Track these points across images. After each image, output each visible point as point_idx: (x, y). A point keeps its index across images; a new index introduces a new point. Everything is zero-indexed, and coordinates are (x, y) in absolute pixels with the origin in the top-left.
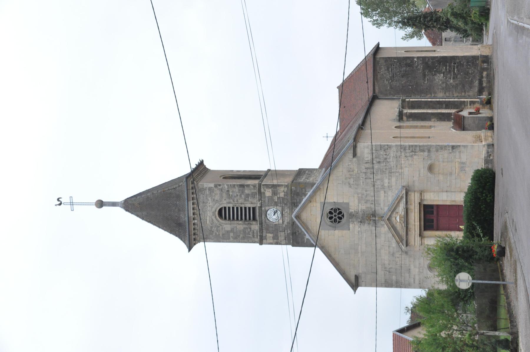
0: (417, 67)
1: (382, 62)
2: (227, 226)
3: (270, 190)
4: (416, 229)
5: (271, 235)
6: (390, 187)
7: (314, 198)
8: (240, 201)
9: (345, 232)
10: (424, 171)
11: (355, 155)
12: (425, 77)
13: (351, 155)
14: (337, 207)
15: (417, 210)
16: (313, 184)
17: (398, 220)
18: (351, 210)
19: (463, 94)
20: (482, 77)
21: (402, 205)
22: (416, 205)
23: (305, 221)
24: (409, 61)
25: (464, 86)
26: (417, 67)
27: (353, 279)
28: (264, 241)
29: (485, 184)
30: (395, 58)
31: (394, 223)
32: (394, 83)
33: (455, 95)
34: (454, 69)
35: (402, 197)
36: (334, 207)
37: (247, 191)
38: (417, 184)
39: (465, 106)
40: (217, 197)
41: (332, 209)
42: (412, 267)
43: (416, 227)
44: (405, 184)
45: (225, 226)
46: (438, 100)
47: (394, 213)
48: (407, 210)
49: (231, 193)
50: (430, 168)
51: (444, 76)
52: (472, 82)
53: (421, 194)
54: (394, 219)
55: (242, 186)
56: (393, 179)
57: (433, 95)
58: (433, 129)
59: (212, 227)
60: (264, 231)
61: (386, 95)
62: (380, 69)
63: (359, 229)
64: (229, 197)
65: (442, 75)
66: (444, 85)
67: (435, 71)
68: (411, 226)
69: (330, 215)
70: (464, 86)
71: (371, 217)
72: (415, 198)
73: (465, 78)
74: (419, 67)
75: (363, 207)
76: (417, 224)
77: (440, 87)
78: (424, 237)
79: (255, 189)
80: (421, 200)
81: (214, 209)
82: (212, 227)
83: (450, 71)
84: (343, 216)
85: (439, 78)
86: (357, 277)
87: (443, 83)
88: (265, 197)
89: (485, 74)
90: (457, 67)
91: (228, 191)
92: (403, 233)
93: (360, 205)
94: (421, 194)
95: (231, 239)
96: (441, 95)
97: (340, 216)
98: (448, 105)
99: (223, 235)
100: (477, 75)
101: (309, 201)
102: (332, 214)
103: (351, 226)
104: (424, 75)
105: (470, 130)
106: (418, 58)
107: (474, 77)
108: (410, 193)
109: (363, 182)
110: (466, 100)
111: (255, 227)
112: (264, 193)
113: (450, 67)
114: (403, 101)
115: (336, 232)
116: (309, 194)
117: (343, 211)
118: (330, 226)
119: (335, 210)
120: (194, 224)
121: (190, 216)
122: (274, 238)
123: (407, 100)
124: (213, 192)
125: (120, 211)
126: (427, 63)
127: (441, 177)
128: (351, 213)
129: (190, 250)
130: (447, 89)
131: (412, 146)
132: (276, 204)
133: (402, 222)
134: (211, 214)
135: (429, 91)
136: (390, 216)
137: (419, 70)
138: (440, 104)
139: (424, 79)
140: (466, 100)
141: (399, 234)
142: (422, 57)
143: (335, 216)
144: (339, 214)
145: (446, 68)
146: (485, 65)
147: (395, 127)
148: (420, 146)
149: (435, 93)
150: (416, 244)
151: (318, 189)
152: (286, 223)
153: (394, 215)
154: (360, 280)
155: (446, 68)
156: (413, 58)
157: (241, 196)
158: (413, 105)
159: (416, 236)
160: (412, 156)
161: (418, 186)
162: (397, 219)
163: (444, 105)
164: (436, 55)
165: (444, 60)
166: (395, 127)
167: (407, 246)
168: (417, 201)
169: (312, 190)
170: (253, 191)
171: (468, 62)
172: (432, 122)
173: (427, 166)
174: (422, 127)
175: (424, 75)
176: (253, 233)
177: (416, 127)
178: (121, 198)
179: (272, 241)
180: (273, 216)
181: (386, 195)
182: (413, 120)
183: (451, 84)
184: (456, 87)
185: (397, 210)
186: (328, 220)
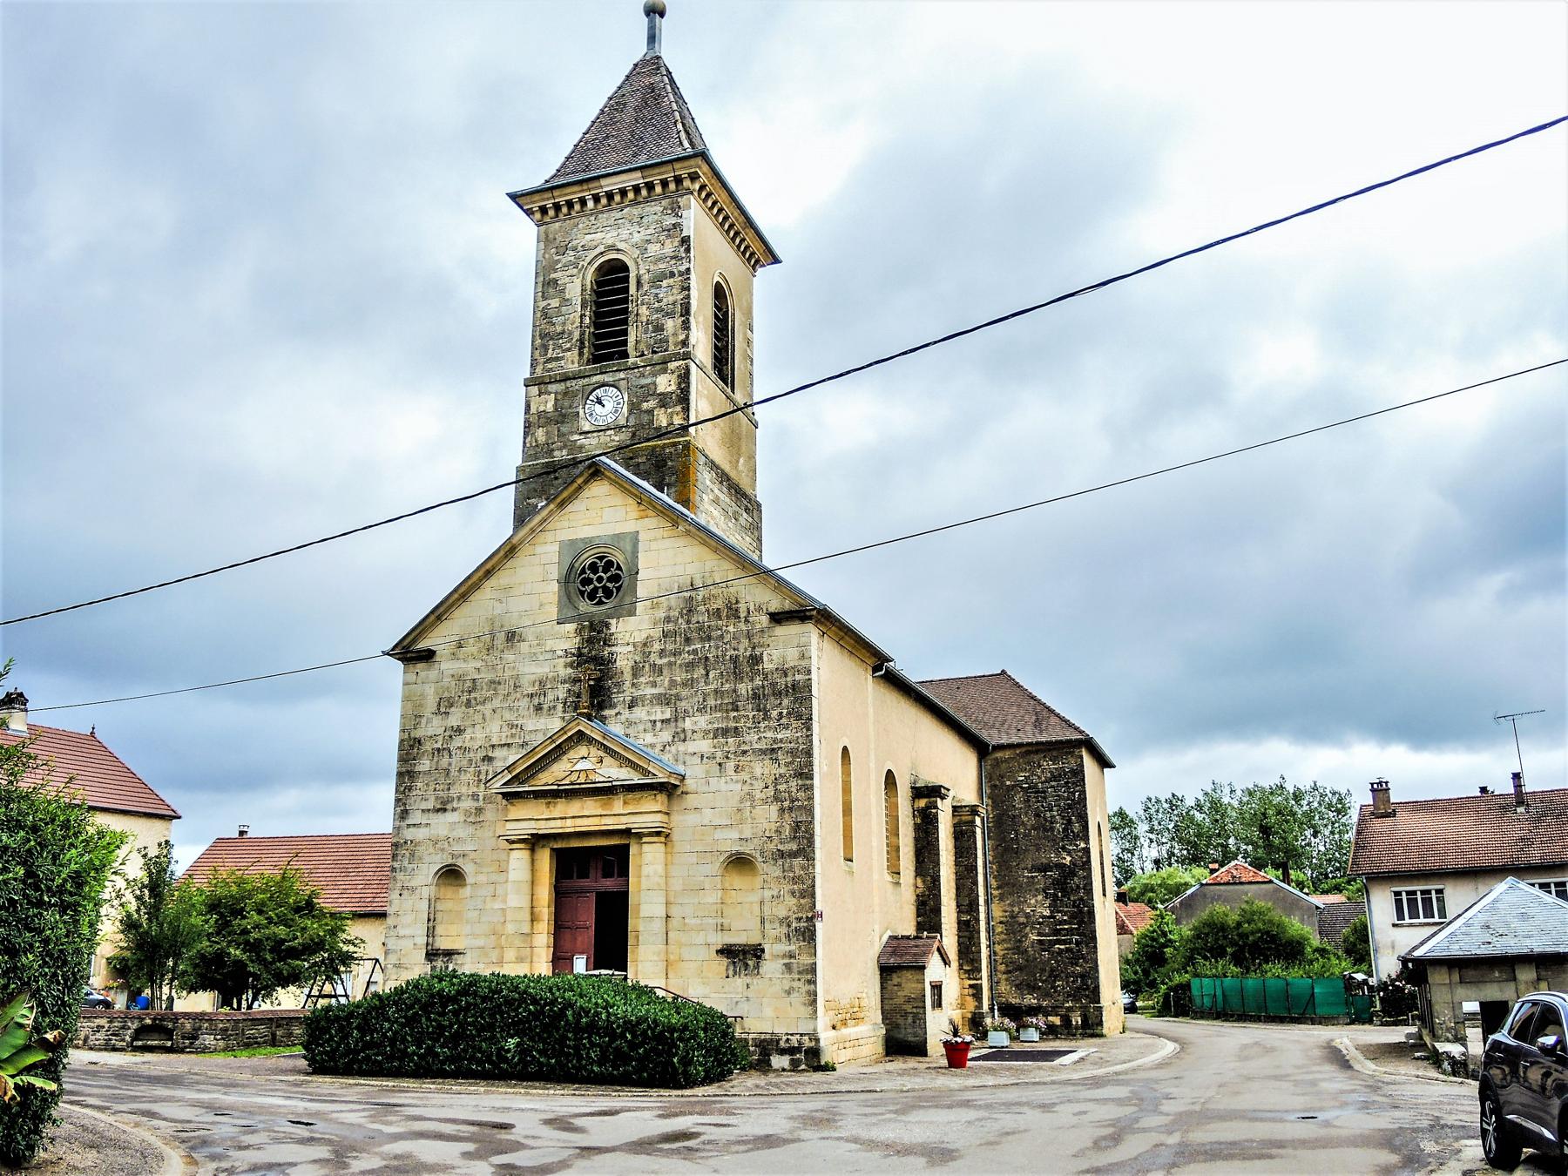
0: (1064, 848)
1: (1073, 763)
2: (577, 286)
3: (674, 387)
4: (552, 824)
5: (550, 407)
6: (681, 736)
7: (650, 513)
8: (644, 310)
9: (553, 612)
10: (729, 842)
11: (778, 618)
12: (1039, 870)
13: (776, 605)
14: (626, 581)
15: (611, 823)
16: (686, 502)
17: (578, 767)
18: (613, 622)
19: (1003, 968)
20: (1046, 1014)
21: (636, 779)
22: (624, 819)
23: (586, 493)
24: (1077, 827)
25: (1020, 968)
26: (1064, 848)
27: (422, 645)
28: (534, 390)
29: (675, 1053)
30: (1083, 792)
31: (572, 754)
32: (1018, 799)
33: (998, 948)
34: (1064, 942)
35: (646, 772)
36: (624, 574)
37: (670, 325)
38: (691, 819)
39: (967, 972)
40: (653, 249)
41: (619, 568)
42: (450, 817)
43: (559, 823)
44: (690, 784)
45: (578, 282)
46: (981, 900)
47: (601, 753)
48: (607, 791)
49: (664, 283)
50: (739, 862)
51: (1043, 917)
52: (1032, 988)
53: (658, 834)
54: (582, 750)
55: (686, 311)
56: (705, 746)
57: (996, 893)
58: (889, 878)
59: (575, 249)
60: (560, 387)
61: (990, 779)
62: (1054, 760)
63: (560, 653)
64: (657, 280)
65: (1047, 913)
66: (1022, 920)
67: (1055, 895)
68: (562, 808)
69: (601, 564)
70: (1020, 968)
71: (595, 686)
72: (644, 813)
73: (1043, 970)
74: (1064, 854)
75: (624, 658)
76: (569, 826)
77: (1016, 909)
78: (533, 850)
79: (676, 345)
80: (639, 836)
81: (621, 246)
82: (575, 249)
83: (1056, 932)
84: (600, 603)
85: (1038, 906)
86: (428, 656)
87: (1027, 916)
88: (655, 375)
89: (1057, 1020)
90: (1068, 950)
91: (672, 275)
92: (545, 780)
93: (630, 648)
94: (658, 834)
95: (542, 304)
96: (997, 912)
97: (600, 594)
98: (967, 931)
99: (555, 281)
100: (1047, 992)
101: (641, 498)
102: (610, 579)
103: (571, 627)
104: (1043, 869)
105: (883, 988)
106: (1087, 851)
107: (1047, 995)
108: (662, 798)
109: (695, 652)
110: (985, 973)
111: (571, 362)
112: (665, 371)
113: (1070, 932)
114: (974, 811)
115: (555, 587)
116: (664, 497)
117: (610, 604)
118: (572, 567)
119: (615, 578)
120: (583, 202)
121: (603, 182)
122: (540, 414)
123: (978, 821)
124: (668, 236)
125: (640, 50)
126: (1073, 874)
127: (712, 897)
128: (607, 626)
129: (514, 197)
130: (1014, 927)
131: (811, 798)
132: (634, 407)
133: (574, 777)
134: (610, 242)
135: (1008, 885)
136: (591, 741)
137: (1058, 854)
138: (967, 905)
139: (1035, 868)
140: (985, 973)
141: (542, 770)
142: (1089, 861)
143: (600, 579)
144: (605, 588)
145: (1065, 922)
146: (1077, 1019)
147: (889, 772)
148: (811, 822)
149: (1002, 898)
150: (510, 825)
151: (674, 519)
152: (583, 441)
153: (595, 752)
154: (420, 666)
155: (1065, 922)
156: (1086, 839)
157: (659, 310)
158: (963, 836)
159: (532, 824)
160: (776, 799)
161: (684, 822)
162: (581, 764)
163: (965, 918)
164: (1095, 897)
165: (1084, 918)
166: (889, 772)
167: (504, 795)
168: (637, 823)
169: (671, 502)
170: (671, 340)
171: (1083, 976)
172: (912, 881)
173: (746, 849)
174: (893, 851)
175: (1043, 869)
176: (557, 359)
177: (893, 831)
178: (670, 54)
179: (533, 410)
180: (607, 409)
181: (659, 724)
182: (917, 828)
183: (1026, 936)
184: (1018, 949)
185: (608, 760)
186: (588, 562)
